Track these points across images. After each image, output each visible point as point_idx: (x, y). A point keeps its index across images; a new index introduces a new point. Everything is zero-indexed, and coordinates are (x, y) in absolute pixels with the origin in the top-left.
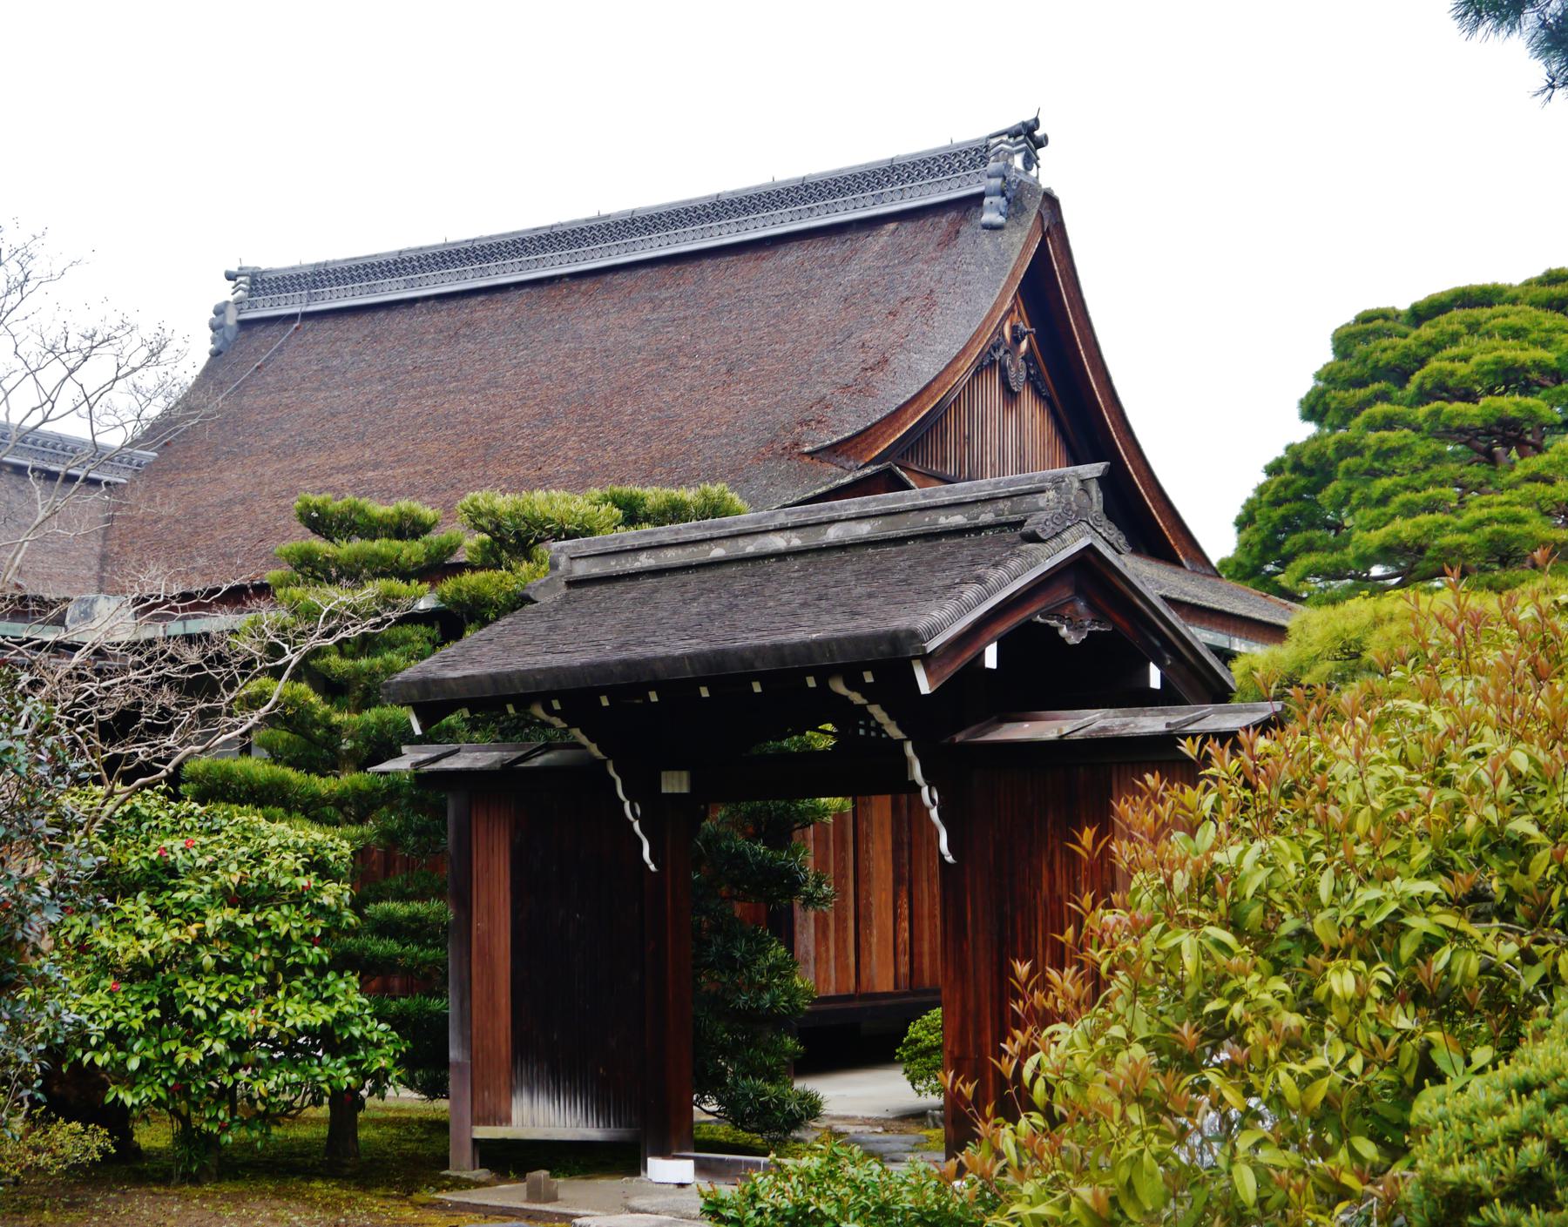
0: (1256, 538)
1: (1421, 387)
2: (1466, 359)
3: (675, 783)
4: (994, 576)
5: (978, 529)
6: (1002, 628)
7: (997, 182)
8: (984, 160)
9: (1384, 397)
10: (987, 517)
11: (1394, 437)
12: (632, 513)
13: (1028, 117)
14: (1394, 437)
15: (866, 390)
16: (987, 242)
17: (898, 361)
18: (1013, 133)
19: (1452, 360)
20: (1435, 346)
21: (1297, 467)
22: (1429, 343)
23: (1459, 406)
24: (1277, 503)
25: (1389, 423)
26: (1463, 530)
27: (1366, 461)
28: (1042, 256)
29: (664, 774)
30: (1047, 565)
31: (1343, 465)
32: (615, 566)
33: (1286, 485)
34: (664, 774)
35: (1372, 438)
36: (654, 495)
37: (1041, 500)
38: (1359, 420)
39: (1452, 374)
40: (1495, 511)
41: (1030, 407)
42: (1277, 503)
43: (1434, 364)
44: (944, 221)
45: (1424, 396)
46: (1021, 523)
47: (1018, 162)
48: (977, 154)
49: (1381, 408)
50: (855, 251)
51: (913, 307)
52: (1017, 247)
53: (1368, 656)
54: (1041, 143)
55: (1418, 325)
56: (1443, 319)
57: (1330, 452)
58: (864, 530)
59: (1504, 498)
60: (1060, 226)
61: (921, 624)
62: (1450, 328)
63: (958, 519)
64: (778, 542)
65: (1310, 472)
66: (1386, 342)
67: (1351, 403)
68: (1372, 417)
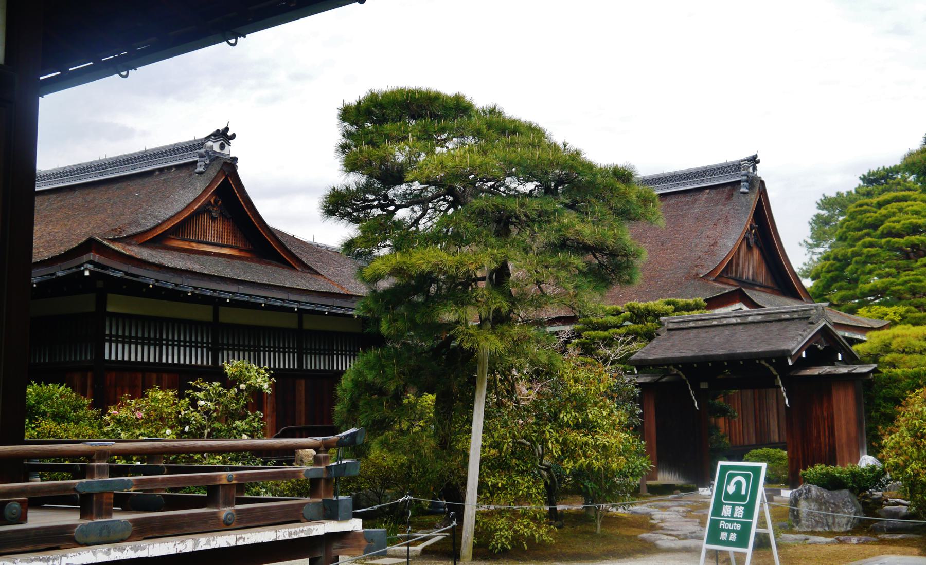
0: (821, 284)
1: (882, 232)
2: (898, 222)
3: (704, 386)
4: (805, 334)
5: (793, 319)
6: (806, 347)
7: (745, 178)
8: (740, 169)
9: (868, 235)
10: (796, 316)
11: (873, 250)
12: (678, 309)
13: (753, 154)
14: (873, 250)
15: (712, 254)
16: (743, 199)
17: (721, 242)
18: (749, 160)
19: (894, 222)
20: (887, 217)
21: (836, 259)
22: (885, 216)
23: (897, 240)
24: (828, 272)
25: (871, 245)
26: (900, 284)
27: (863, 258)
28: (760, 201)
29: (109, 296)
30: (816, 330)
31: (854, 259)
32: (682, 326)
33: (832, 265)
34: (109, 296)
35: (865, 250)
36: (681, 301)
37: (812, 312)
38: (860, 243)
39: (894, 228)
40: (911, 277)
41: (756, 253)
42: (828, 272)
43: (887, 224)
44: (727, 189)
45: (883, 236)
46: (808, 318)
47: (751, 170)
48: (736, 167)
49: (868, 239)
50: (696, 200)
51: (721, 222)
52: (753, 198)
53: (892, 347)
54: (758, 162)
55: (880, 208)
56: (889, 206)
57: (849, 254)
58: (759, 318)
59: (914, 273)
60: (765, 190)
61: (790, 348)
62: (893, 210)
63: (787, 316)
64: (734, 321)
65: (839, 261)
66: (868, 215)
67: (857, 237)
68: (865, 243)
